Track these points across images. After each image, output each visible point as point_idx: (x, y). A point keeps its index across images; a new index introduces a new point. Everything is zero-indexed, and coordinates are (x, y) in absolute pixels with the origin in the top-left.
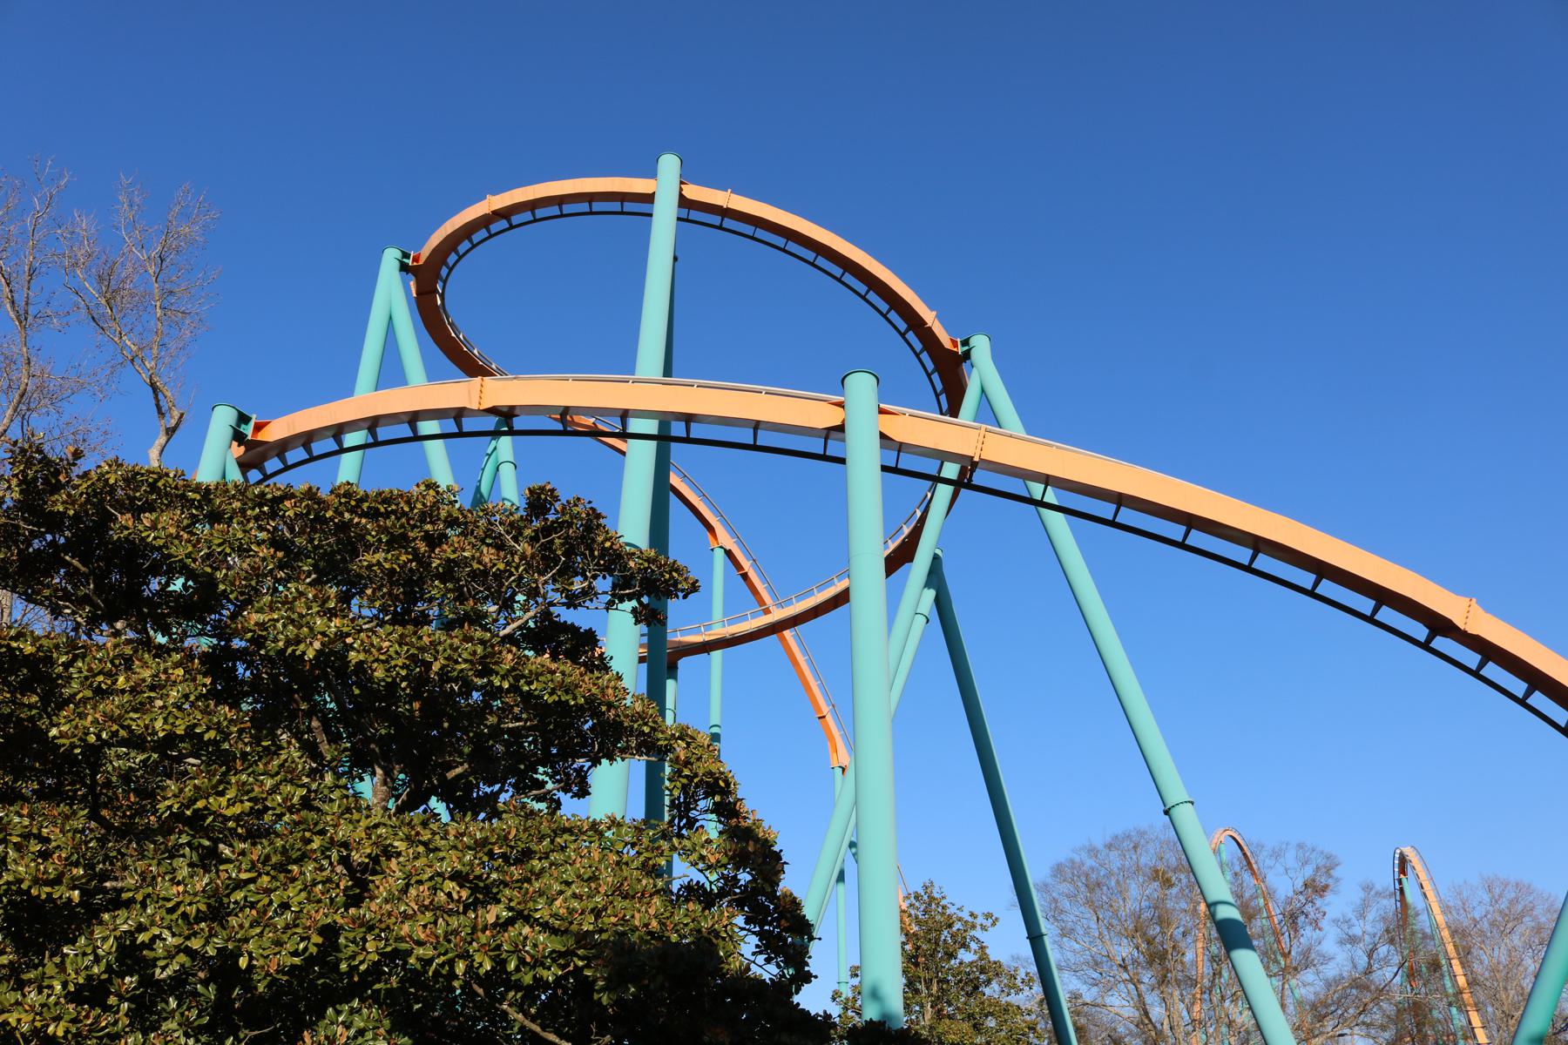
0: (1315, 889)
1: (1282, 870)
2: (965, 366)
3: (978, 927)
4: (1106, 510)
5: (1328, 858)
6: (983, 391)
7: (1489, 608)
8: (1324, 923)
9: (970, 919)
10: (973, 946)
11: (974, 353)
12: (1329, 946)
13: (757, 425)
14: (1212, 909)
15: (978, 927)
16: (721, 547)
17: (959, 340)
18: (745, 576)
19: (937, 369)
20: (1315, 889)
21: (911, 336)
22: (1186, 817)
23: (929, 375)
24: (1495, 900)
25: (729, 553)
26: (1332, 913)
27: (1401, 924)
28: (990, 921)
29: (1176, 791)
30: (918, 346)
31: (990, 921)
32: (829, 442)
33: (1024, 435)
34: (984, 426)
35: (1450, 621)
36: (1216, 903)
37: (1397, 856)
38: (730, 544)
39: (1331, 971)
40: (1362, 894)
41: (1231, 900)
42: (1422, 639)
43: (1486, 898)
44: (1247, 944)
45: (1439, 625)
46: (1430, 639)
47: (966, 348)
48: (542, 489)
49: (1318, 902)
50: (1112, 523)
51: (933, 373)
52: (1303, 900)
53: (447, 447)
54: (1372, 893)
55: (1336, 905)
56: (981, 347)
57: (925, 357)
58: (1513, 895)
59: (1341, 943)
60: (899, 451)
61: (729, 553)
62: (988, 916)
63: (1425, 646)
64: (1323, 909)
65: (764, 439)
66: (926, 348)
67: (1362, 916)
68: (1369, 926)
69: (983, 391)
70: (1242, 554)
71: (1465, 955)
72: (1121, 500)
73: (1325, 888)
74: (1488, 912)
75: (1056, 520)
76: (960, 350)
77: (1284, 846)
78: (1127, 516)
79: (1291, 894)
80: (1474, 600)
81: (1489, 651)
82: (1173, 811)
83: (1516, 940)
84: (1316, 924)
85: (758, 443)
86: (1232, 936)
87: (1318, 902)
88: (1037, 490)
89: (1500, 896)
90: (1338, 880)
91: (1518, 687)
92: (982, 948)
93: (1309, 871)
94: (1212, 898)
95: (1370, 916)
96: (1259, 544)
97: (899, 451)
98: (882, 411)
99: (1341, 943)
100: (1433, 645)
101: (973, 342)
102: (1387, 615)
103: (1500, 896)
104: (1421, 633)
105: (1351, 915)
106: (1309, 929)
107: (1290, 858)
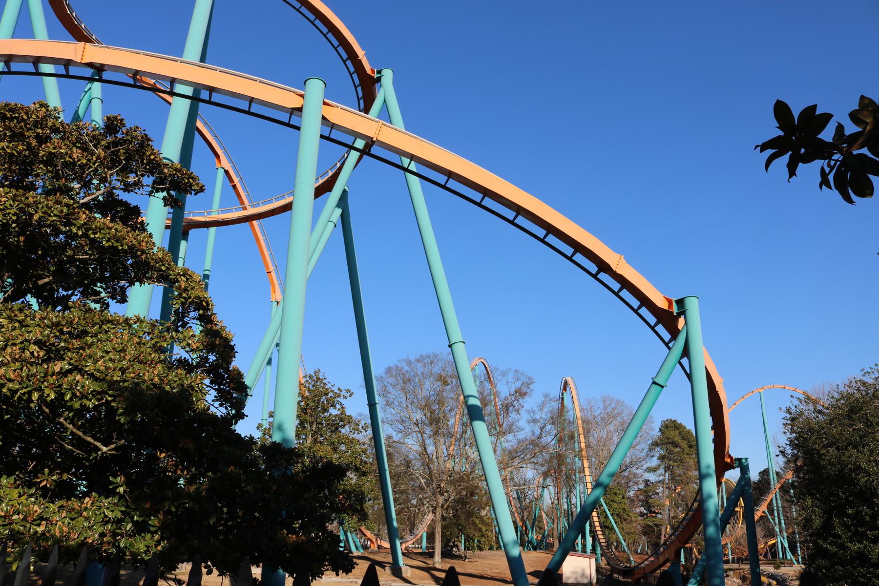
0: (520, 393)
1: (505, 382)
2: (377, 85)
3: (342, 397)
4: (441, 179)
5: (530, 378)
6: (385, 101)
7: (629, 261)
8: (522, 412)
9: (338, 392)
10: (338, 406)
11: (383, 79)
12: (522, 423)
13: (252, 100)
14: (466, 399)
15: (342, 397)
16: (223, 168)
17: (376, 70)
18: (234, 187)
19: (360, 84)
20: (520, 393)
21: (349, 63)
22: (460, 349)
23: (351, 75)
24: (605, 407)
25: (227, 172)
26: (527, 406)
27: (559, 416)
28: (349, 394)
29: (456, 335)
30: (352, 69)
31: (349, 394)
32: (333, 130)
33: (403, 130)
34: (381, 121)
35: (609, 265)
36: (469, 396)
37: (563, 381)
38: (228, 167)
39: (521, 436)
40: (543, 399)
41: (476, 395)
42: (594, 272)
43: (602, 406)
44: (482, 419)
45: (604, 267)
46: (598, 273)
47: (379, 75)
48: (115, 118)
49: (521, 401)
50: (444, 187)
51: (361, 99)
52: (513, 398)
53: (55, 67)
54: (548, 398)
55: (529, 403)
56: (388, 76)
57: (355, 76)
58: (614, 406)
59: (529, 422)
60: (332, 128)
61: (227, 172)
62: (348, 391)
63: (595, 276)
64: (523, 404)
65: (255, 109)
66: (356, 71)
67: (541, 410)
68: (543, 415)
69: (385, 101)
70: (510, 214)
71: (587, 434)
72: (450, 174)
73: (525, 394)
74: (601, 413)
75: (414, 181)
76: (376, 76)
77: (508, 371)
78: (453, 184)
79: (508, 395)
80: (623, 256)
81: (625, 284)
82: (454, 346)
83: (612, 428)
84: (518, 412)
85: (251, 111)
86: (474, 413)
87: (521, 401)
88: (406, 162)
89: (609, 405)
90: (532, 390)
91: (635, 303)
92: (343, 408)
93: (518, 384)
94: (467, 393)
95: (545, 410)
96: (520, 210)
97: (332, 128)
98: (325, 104)
99: (529, 422)
100: (599, 276)
101: (383, 72)
102: (551, 239)
103: (609, 405)
104: (594, 269)
105: (536, 409)
106: (514, 413)
107: (510, 377)
